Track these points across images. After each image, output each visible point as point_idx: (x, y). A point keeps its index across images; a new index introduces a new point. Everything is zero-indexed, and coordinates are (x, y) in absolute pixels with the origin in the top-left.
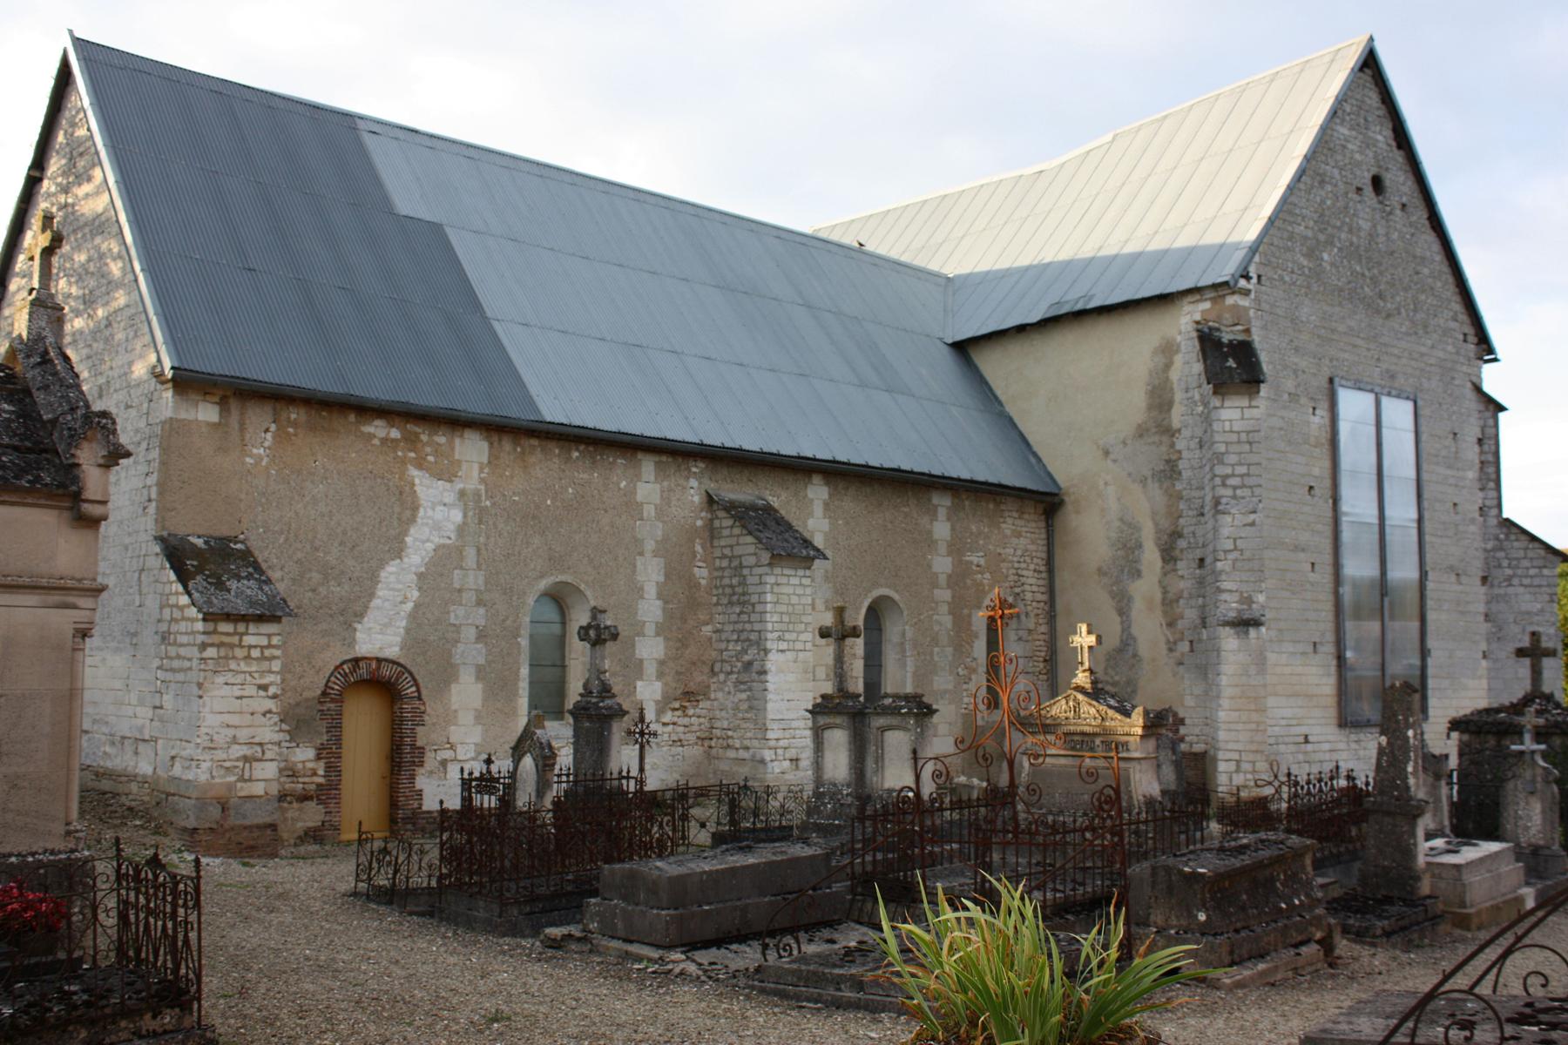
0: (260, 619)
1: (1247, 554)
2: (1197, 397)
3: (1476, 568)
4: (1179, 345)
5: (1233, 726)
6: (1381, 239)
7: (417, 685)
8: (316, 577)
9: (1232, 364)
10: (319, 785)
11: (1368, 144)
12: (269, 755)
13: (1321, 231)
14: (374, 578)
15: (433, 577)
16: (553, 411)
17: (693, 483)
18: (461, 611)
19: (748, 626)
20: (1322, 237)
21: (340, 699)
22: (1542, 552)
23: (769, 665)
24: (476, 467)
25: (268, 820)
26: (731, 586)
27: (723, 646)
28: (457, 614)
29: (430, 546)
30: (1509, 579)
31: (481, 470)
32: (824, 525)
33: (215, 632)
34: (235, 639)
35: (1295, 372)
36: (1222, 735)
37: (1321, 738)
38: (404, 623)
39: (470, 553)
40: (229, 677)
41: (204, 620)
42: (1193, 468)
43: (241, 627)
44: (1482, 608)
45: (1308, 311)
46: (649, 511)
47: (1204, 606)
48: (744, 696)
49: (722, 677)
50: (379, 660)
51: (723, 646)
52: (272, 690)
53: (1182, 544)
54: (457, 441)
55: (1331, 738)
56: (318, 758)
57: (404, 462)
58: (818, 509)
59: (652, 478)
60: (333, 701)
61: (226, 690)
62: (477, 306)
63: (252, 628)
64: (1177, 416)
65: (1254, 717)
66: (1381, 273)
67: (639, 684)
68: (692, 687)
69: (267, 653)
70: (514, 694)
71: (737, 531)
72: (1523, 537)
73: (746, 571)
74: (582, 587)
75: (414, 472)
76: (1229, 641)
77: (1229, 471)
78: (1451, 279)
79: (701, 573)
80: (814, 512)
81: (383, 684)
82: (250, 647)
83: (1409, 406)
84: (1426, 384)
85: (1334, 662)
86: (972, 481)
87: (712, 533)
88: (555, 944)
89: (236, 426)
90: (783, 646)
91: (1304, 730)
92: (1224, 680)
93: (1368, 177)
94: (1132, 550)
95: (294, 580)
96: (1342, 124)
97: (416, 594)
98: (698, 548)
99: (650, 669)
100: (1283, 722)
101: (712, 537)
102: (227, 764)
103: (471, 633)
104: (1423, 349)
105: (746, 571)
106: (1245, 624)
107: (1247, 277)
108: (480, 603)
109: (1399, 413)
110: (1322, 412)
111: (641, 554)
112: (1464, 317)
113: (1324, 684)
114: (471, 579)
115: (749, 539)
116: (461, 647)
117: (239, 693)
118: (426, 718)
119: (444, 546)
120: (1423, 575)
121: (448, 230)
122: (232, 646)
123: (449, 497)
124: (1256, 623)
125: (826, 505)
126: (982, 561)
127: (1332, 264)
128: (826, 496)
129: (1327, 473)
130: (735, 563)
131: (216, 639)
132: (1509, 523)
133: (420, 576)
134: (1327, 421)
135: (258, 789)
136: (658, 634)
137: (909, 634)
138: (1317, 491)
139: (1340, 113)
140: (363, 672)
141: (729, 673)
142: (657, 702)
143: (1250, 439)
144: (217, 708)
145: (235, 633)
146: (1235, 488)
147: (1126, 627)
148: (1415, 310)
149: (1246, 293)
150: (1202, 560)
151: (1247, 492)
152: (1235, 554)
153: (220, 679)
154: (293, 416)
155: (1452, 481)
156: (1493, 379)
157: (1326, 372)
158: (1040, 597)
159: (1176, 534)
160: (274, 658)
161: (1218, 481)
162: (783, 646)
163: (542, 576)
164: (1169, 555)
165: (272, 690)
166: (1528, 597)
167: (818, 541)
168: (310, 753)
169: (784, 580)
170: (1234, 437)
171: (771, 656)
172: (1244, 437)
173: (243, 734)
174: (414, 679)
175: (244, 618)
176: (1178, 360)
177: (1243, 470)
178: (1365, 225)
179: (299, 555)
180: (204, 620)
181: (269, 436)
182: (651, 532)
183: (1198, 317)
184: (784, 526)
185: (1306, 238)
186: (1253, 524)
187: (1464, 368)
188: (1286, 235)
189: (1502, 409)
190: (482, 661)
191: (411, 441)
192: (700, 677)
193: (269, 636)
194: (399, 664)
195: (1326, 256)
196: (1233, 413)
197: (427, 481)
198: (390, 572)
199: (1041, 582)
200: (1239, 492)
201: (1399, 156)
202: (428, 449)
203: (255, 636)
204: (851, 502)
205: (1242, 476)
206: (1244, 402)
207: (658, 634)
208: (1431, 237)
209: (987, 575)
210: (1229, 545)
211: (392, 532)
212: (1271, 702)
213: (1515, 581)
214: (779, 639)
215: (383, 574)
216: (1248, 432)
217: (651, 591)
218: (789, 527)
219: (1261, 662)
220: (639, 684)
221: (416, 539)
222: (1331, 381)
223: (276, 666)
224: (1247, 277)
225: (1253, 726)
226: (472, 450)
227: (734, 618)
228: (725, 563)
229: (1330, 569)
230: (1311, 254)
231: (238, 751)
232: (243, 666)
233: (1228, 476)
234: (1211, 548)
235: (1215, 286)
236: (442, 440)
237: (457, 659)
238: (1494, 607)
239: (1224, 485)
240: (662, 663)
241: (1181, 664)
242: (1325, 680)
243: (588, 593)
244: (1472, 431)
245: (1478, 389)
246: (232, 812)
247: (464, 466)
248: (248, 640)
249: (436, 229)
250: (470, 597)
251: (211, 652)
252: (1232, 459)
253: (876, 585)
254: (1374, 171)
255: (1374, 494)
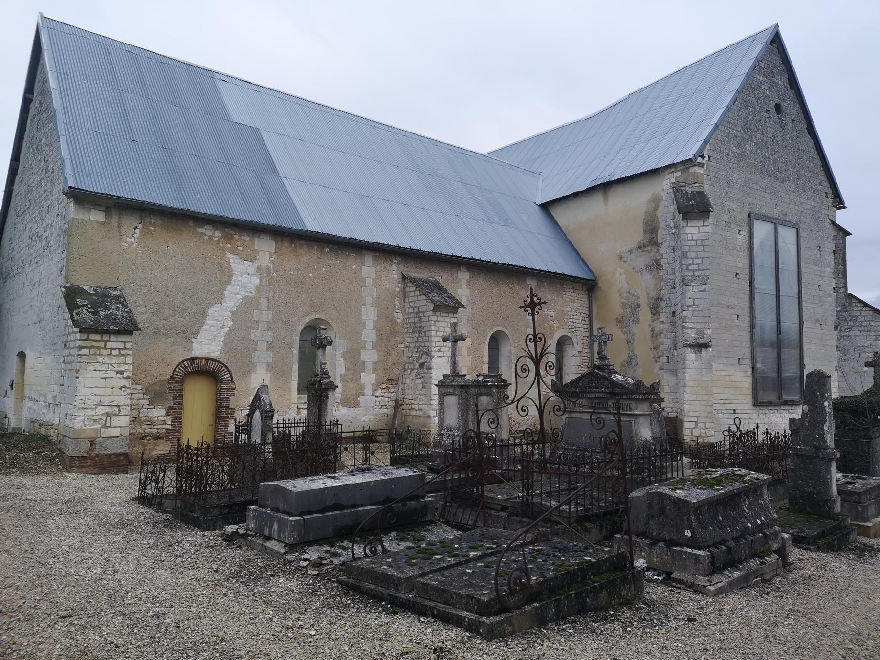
0: (119, 332)
1: (701, 308)
2: (672, 224)
3: (832, 319)
4: (662, 197)
5: (692, 403)
6: (780, 139)
7: (231, 374)
8: (167, 312)
9: (694, 207)
10: (167, 430)
11: (773, 85)
12: (123, 412)
13: (745, 132)
14: (204, 314)
15: (244, 312)
16: (312, 225)
17: (394, 268)
18: (258, 333)
19: (422, 344)
20: (746, 136)
21: (182, 382)
22: (871, 313)
23: (433, 364)
24: (267, 255)
25: (122, 450)
26: (414, 323)
27: (410, 354)
28: (255, 335)
29: (239, 297)
30: (851, 328)
31: (271, 256)
32: (467, 292)
33: (87, 340)
34: (102, 344)
35: (729, 210)
36: (686, 407)
37: (744, 411)
38: (223, 339)
39: (264, 301)
40: (97, 366)
41: (80, 332)
42: (669, 263)
43: (106, 337)
44: (835, 343)
45: (737, 177)
46: (369, 282)
47: (675, 337)
48: (420, 381)
49: (409, 371)
50: (207, 359)
51: (410, 354)
52: (126, 374)
53: (663, 304)
54: (256, 239)
55: (749, 411)
56: (167, 414)
57: (223, 250)
58: (464, 284)
59: (371, 264)
60: (177, 382)
61: (96, 374)
62: (274, 170)
63: (113, 338)
64: (661, 234)
65: (706, 398)
66: (779, 157)
67: (362, 374)
68: (392, 377)
69: (123, 352)
70: (288, 380)
71: (417, 293)
72: (859, 304)
73: (421, 314)
74: (330, 322)
75: (230, 255)
76: (690, 355)
77: (690, 261)
78: (819, 163)
79: (399, 316)
80: (462, 286)
81: (209, 372)
82: (112, 349)
83: (795, 230)
84: (803, 219)
85: (750, 370)
86: (548, 272)
87: (404, 294)
88: (230, 539)
89: (116, 224)
90: (441, 354)
91: (734, 407)
92: (688, 377)
93: (773, 104)
94: (635, 308)
95: (153, 314)
96: (759, 74)
97: (231, 323)
98: (397, 303)
99: (369, 367)
100: (722, 402)
101: (405, 297)
102: (95, 418)
103: (264, 345)
104: (802, 200)
105: (421, 314)
106: (700, 346)
107: (703, 157)
108: (269, 329)
109: (787, 236)
110: (744, 233)
111: (364, 305)
112: (826, 184)
113: (745, 381)
114: (264, 315)
115: (423, 297)
116: (257, 353)
117: (104, 376)
118: (236, 392)
119: (248, 297)
120: (801, 323)
121: (262, 132)
122: (99, 348)
123: (252, 270)
124: (706, 346)
125: (468, 283)
126: (553, 314)
127: (751, 152)
128: (468, 277)
129: (747, 266)
130: (416, 310)
131: (88, 344)
132: (850, 295)
133: (233, 313)
134: (747, 238)
135: (116, 432)
136: (373, 348)
137: (513, 351)
138: (740, 276)
139: (758, 67)
140: (197, 365)
141: (412, 370)
142: (373, 385)
143: (703, 243)
144: (88, 385)
145: (101, 341)
146: (694, 271)
147: (631, 350)
148: (798, 179)
149: (701, 165)
150: (674, 313)
151: (700, 273)
152: (694, 308)
153: (91, 367)
154: (153, 221)
155: (817, 273)
156: (842, 218)
157: (747, 211)
158: (584, 334)
159: (659, 299)
160: (128, 355)
161: (684, 267)
162: (441, 354)
163: (307, 315)
164: (655, 310)
165: (126, 374)
166: (861, 338)
167: (464, 301)
168: (163, 412)
169: (442, 319)
170: (694, 243)
171: (433, 360)
172: (699, 243)
173: (106, 400)
174: (229, 371)
175: (109, 332)
176: (662, 205)
177: (699, 261)
178: (771, 131)
179: (157, 299)
180: (80, 332)
181: (137, 231)
182: (370, 293)
183: (673, 180)
184: (441, 290)
185: (736, 136)
186: (704, 291)
187: (826, 212)
188: (725, 134)
189: (848, 234)
190: (270, 361)
191: (227, 238)
192: (396, 372)
193: (125, 342)
194: (219, 362)
195: (747, 147)
196: (693, 230)
197: (238, 261)
198: (214, 311)
199: (585, 326)
200: (696, 273)
201: (791, 93)
202: (239, 243)
203: (115, 343)
204: (482, 282)
205: (698, 264)
206: (700, 223)
207: (373, 348)
208: (808, 138)
209: (556, 322)
210: (690, 302)
211: (216, 288)
212: (715, 390)
213: (855, 329)
214: (439, 351)
215: (210, 311)
216: (702, 240)
217: (370, 325)
218: (446, 291)
219: (709, 369)
220: (362, 374)
221: (230, 293)
222: (749, 215)
223: (129, 360)
224: (703, 157)
225: (705, 403)
226: (265, 247)
227: (415, 339)
228: (411, 311)
229: (748, 319)
230: (739, 145)
231: (101, 410)
232: (107, 360)
233: (690, 265)
234: (679, 305)
235: (684, 162)
236: (247, 238)
237: (255, 360)
238: (842, 342)
239: (687, 269)
240: (376, 363)
241: (662, 369)
242: (744, 379)
243: (334, 325)
244: (830, 246)
245: (834, 224)
246: (97, 446)
247: (261, 253)
248: (109, 345)
249: (255, 131)
250: (263, 326)
251: (85, 351)
252: (693, 255)
253: (496, 325)
254: (777, 100)
255: (774, 280)
